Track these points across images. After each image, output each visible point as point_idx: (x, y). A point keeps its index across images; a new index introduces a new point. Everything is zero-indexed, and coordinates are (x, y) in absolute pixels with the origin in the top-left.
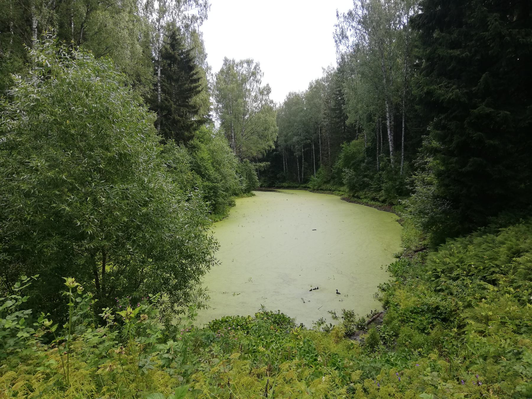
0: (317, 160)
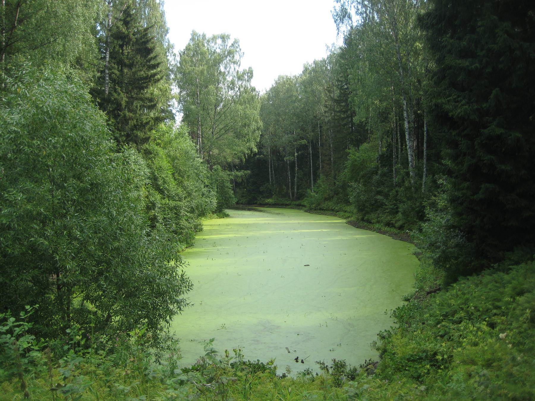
0: (316, 169)
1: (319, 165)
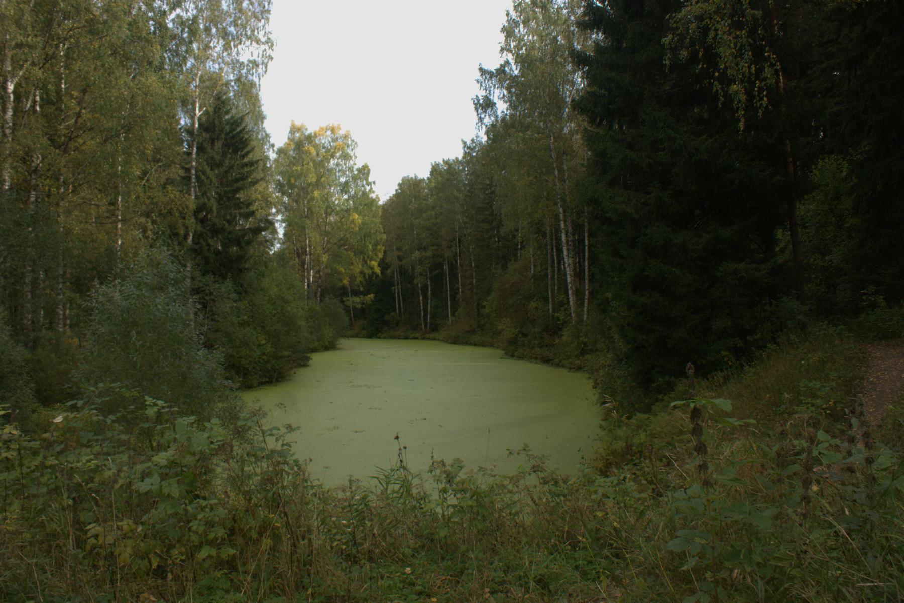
1: (458, 288)
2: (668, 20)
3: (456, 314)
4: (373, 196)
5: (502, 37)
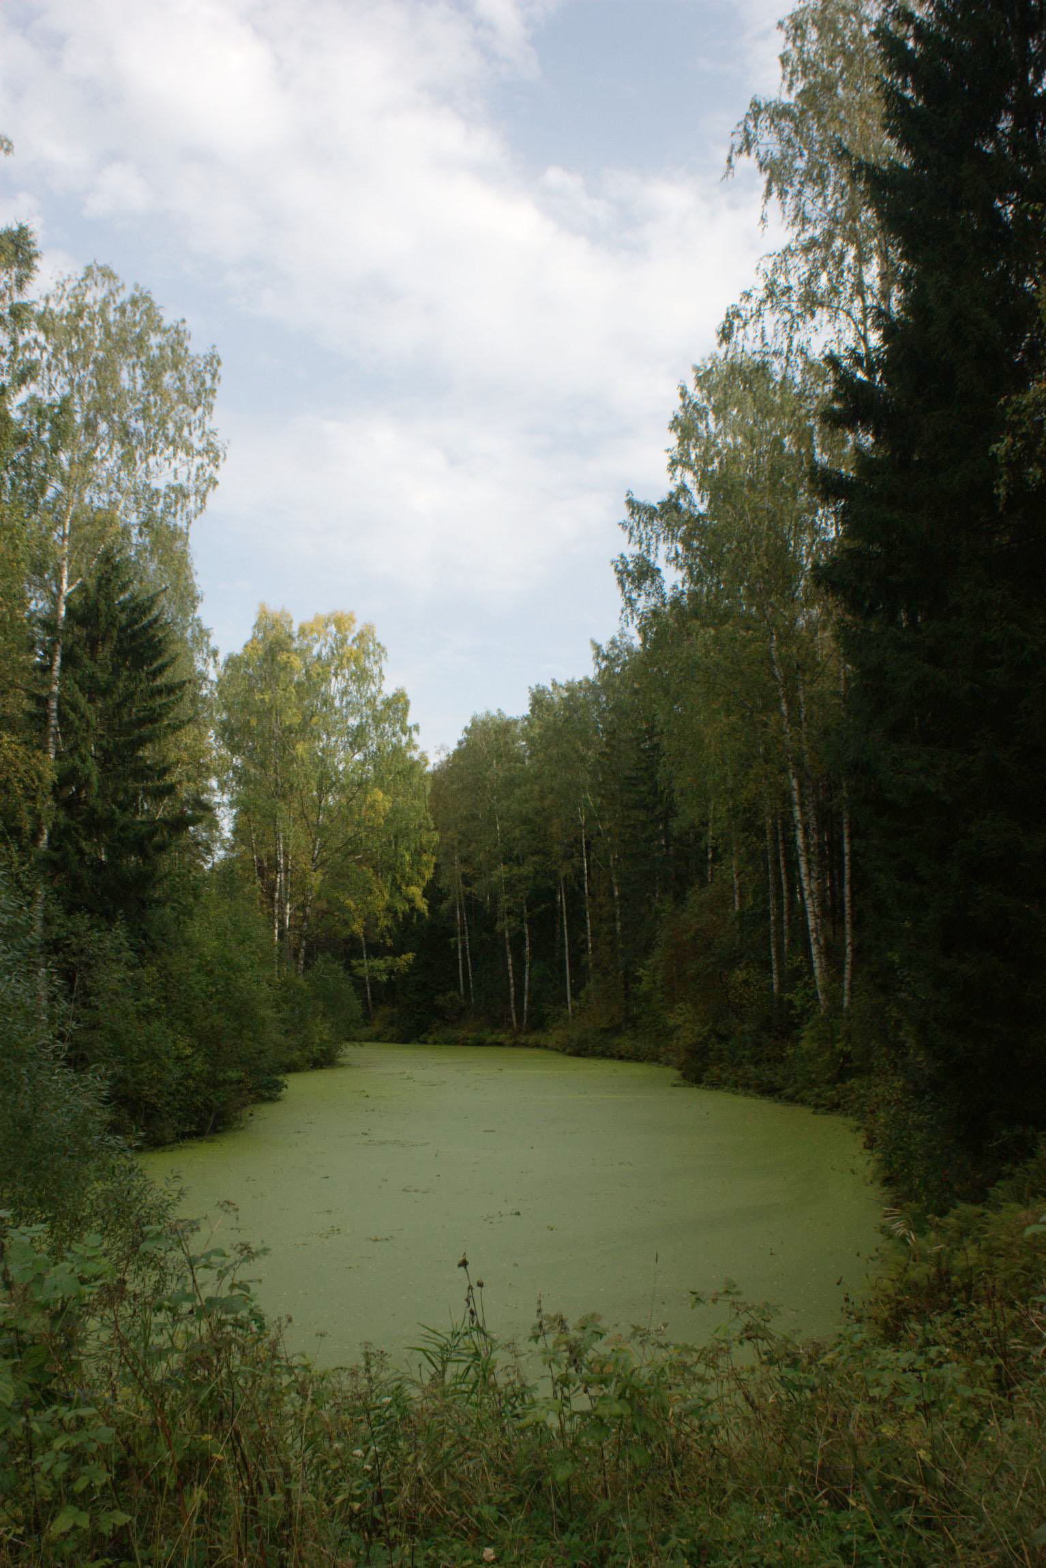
1: (585, 941)
2: (1003, 408)
3: (582, 994)
4: (416, 755)
5: (672, 440)
